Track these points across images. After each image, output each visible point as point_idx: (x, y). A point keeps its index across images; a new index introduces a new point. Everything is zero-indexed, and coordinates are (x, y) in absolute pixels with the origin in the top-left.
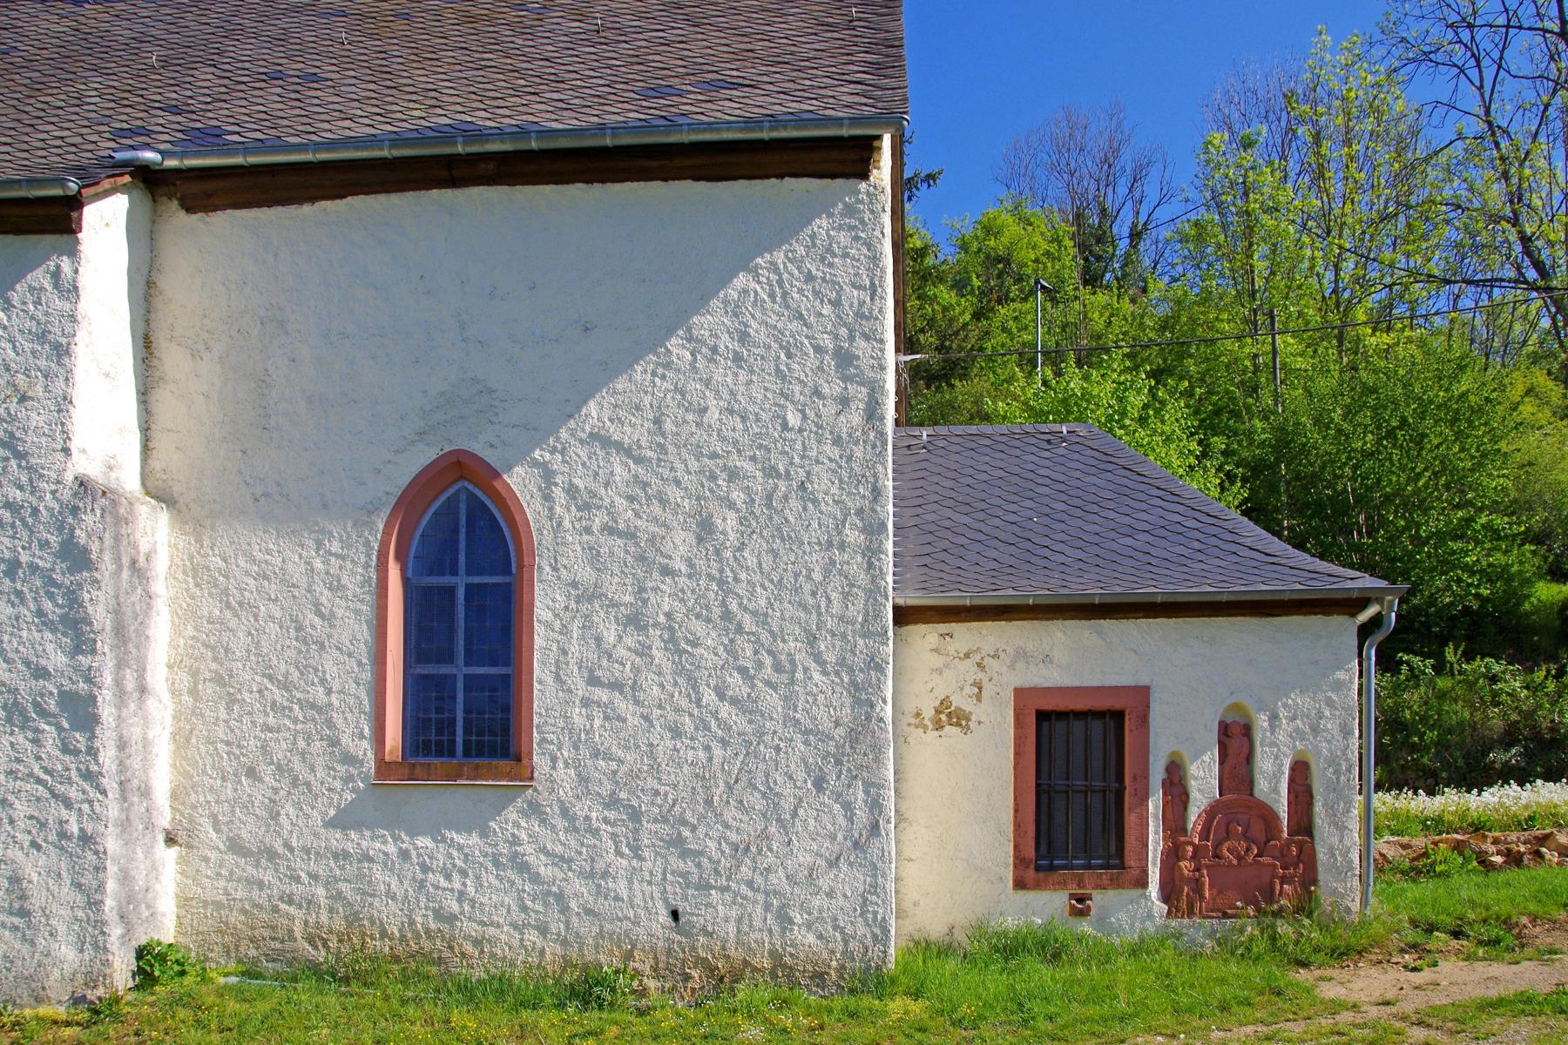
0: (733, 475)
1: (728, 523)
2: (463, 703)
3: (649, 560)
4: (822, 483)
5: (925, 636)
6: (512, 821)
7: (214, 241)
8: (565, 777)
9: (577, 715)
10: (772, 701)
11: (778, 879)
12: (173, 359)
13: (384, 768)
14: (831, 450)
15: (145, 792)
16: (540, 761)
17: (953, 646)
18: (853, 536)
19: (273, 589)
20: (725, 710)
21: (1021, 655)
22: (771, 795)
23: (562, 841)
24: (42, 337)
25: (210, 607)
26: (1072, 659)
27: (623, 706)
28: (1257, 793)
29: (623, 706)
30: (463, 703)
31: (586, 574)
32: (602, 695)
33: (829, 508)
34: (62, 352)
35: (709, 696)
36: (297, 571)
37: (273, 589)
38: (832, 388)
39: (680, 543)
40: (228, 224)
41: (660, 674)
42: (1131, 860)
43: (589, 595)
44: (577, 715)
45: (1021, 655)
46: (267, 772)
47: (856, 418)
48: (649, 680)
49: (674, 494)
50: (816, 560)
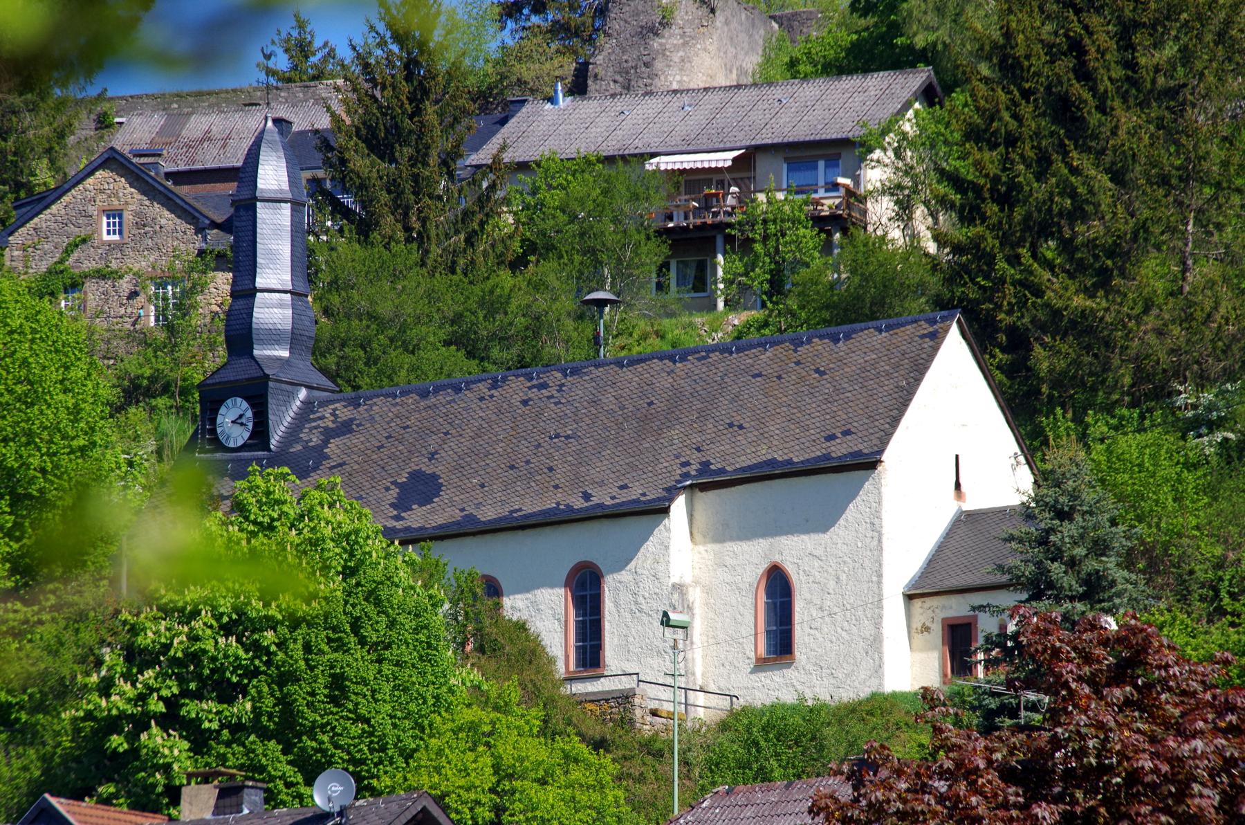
0: (845, 562)
1: (844, 577)
2: (780, 644)
3: (825, 591)
4: (867, 563)
5: (917, 603)
6: (790, 673)
7: (706, 500)
8: (803, 657)
9: (806, 639)
10: (855, 630)
11: (856, 684)
12: (695, 532)
13: (758, 660)
14: (869, 553)
15: (693, 674)
16: (797, 653)
17: (927, 605)
18: (875, 579)
19: (727, 608)
20: (844, 634)
21: (944, 607)
22: (855, 658)
23: (804, 678)
24: (662, 544)
25: (711, 615)
26: (958, 607)
27: (818, 635)
28: (240, 164)
29: (818, 635)
30: (780, 644)
31: (808, 596)
32: (812, 632)
33: (869, 570)
34: (667, 548)
35: (839, 630)
36: (734, 602)
37: (727, 608)
38: (870, 534)
39: (832, 584)
40: (711, 495)
41: (335, 629)
42: (966, 621)
43: (809, 602)
44: (806, 639)
45: (944, 607)
46: (727, 664)
47: (875, 543)
48: (824, 626)
49: (830, 570)
50: (865, 586)
